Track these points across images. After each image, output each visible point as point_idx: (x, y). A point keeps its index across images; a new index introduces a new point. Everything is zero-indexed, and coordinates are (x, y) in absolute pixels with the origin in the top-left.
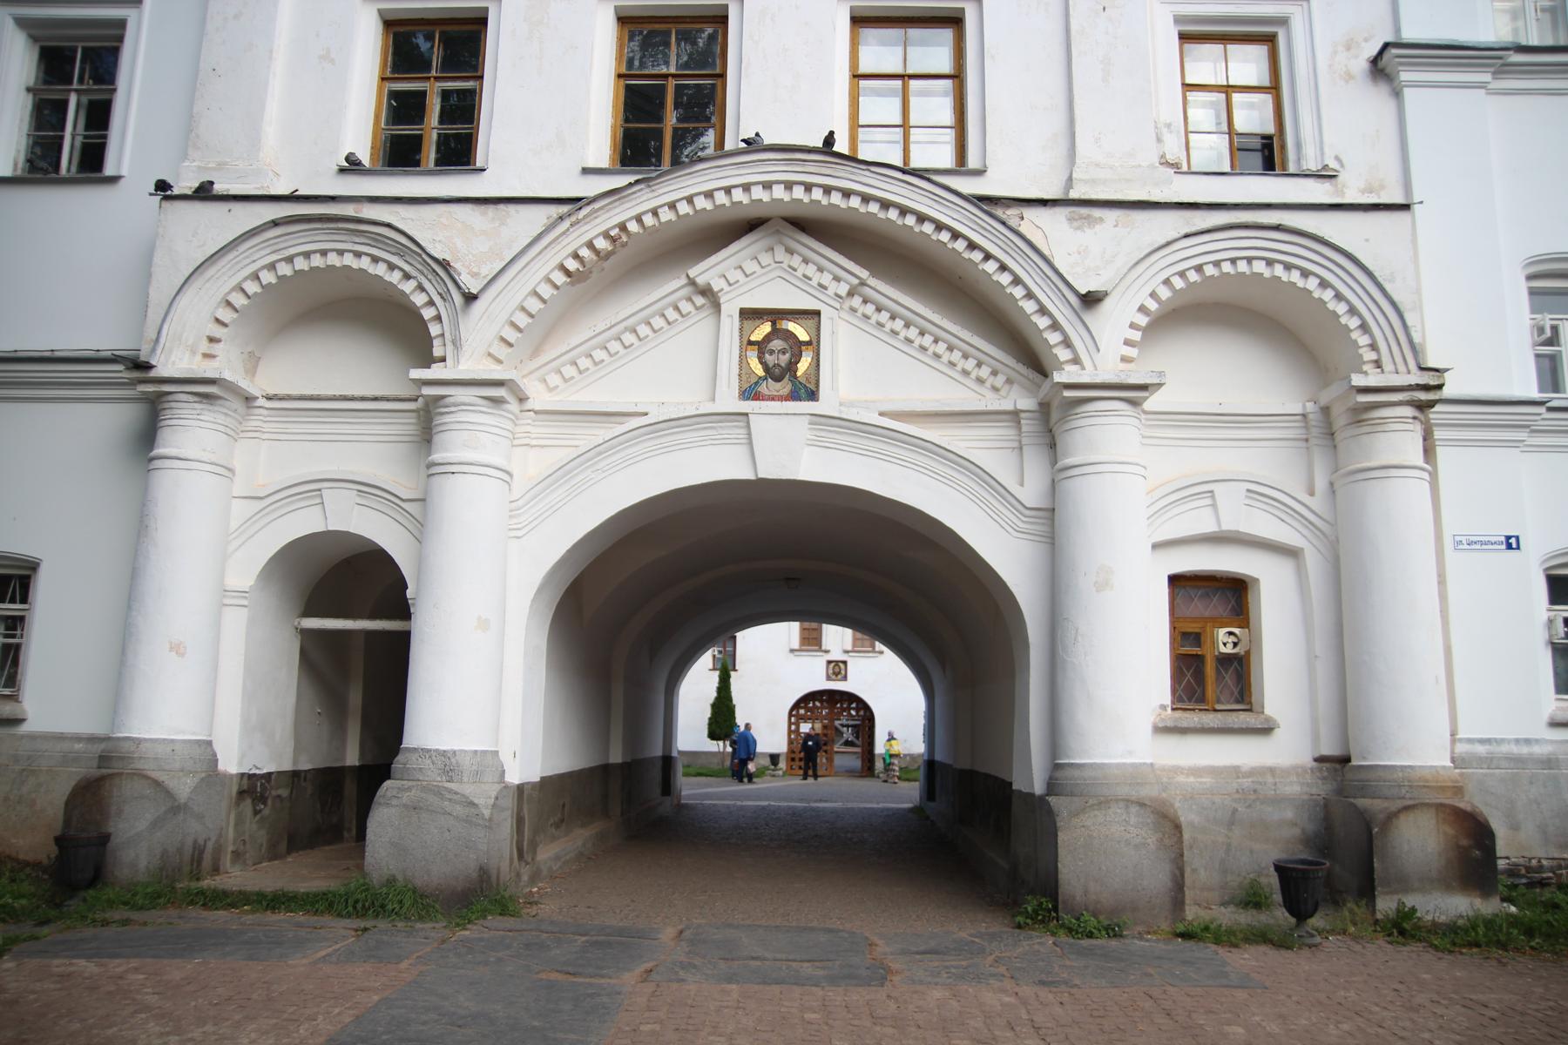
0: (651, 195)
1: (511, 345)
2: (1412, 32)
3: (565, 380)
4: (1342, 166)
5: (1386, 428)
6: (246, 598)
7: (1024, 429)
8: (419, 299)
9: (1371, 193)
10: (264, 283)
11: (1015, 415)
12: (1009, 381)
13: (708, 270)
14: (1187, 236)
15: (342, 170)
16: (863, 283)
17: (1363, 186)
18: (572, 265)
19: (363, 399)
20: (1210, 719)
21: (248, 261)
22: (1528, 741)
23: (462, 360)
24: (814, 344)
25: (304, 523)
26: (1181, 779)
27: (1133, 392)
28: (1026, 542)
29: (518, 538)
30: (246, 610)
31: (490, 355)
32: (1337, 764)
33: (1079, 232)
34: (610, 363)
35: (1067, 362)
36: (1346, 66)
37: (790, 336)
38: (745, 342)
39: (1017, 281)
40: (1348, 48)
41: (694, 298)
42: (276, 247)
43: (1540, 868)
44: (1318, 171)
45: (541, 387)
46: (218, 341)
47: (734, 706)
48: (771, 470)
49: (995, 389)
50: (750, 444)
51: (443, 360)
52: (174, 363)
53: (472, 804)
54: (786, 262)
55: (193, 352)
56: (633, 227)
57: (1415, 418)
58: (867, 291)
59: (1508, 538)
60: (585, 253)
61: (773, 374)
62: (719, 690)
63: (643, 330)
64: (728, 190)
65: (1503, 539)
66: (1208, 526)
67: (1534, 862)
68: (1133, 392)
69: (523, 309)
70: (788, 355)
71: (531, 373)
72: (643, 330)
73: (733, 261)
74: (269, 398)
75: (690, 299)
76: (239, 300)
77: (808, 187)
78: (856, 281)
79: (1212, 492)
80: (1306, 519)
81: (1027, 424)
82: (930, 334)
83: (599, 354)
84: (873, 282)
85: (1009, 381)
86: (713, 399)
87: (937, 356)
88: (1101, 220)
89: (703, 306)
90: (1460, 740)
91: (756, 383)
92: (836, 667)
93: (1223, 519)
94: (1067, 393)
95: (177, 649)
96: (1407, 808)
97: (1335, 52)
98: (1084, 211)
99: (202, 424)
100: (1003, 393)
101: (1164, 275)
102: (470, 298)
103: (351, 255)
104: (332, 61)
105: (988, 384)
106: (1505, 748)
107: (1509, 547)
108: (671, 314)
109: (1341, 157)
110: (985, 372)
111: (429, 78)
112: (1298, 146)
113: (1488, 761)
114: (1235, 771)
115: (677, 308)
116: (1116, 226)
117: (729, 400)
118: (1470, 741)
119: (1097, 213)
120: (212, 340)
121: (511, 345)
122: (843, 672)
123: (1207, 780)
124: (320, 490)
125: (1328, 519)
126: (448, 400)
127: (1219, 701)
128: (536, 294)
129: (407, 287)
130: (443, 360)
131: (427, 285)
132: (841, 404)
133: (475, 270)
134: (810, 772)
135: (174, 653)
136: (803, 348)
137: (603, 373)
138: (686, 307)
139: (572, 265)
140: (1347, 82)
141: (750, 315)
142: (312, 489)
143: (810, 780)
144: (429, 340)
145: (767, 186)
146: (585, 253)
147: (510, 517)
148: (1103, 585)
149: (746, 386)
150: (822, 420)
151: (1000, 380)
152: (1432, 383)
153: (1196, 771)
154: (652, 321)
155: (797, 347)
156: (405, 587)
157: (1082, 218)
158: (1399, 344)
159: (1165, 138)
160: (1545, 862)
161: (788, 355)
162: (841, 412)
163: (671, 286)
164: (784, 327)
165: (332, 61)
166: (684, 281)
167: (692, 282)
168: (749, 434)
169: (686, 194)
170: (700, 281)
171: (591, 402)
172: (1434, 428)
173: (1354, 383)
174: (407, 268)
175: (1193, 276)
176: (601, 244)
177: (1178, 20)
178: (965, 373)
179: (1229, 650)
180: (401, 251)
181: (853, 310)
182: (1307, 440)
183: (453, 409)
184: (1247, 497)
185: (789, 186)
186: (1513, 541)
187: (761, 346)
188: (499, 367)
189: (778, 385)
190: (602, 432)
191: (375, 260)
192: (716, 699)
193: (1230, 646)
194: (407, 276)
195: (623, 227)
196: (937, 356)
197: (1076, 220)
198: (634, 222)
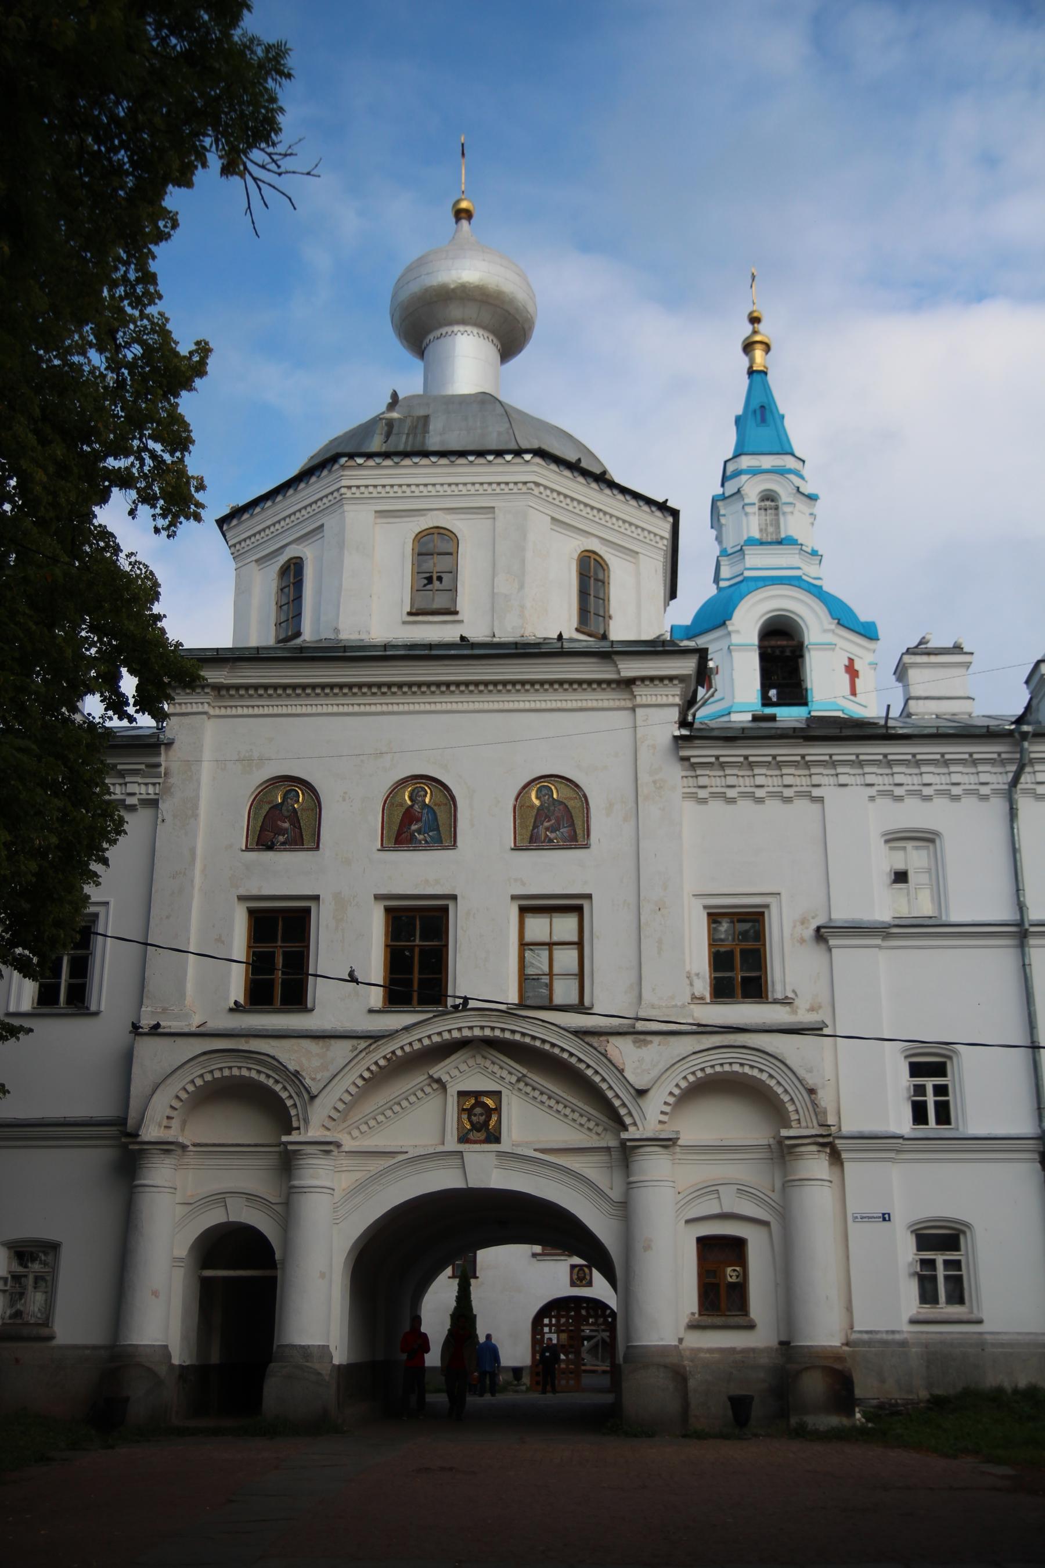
0: (408, 1035)
1: (334, 1120)
2: (841, 914)
3: (361, 1133)
4: (796, 995)
5: (803, 1157)
6: (183, 1262)
7: (613, 1157)
8: (284, 1095)
9: (813, 1011)
10: (197, 1085)
11: (608, 1149)
12: (605, 1129)
13: (439, 1070)
14: (694, 1053)
15: (231, 1010)
16: (524, 1076)
17: (808, 1007)
18: (367, 1075)
19: (249, 1145)
20: (718, 1320)
21: (188, 1074)
22: (893, 1332)
23: (309, 1131)
24: (498, 1110)
25: (215, 1217)
26: (702, 1355)
27: (668, 1143)
28: (613, 1220)
29: (337, 1224)
30: (182, 1269)
31: (323, 1126)
32: (785, 1345)
33: (639, 1050)
34: (386, 1123)
35: (631, 1124)
36: (801, 934)
37: (485, 1106)
38: (460, 1109)
39: (604, 1080)
40: (802, 923)
41: (432, 1085)
42: (204, 1066)
43: (897, 1405)
44: (783, 999)
45: (348, 1137)
46: (172, 1118)
47: (475, 1316)
48: (474, 1183)
49: (598, 1134)
50: (464, 1167)
51: (298, 1128)
52: (150, 1133)
53: (319, 1374)
54: (482, 1064)
55: (160, 1126)
56: (399, 1053)
57: (819, 1151)
58: (527, 1079)
59: (884, 1214)
60: (374, 1068)
61: (477, 1128)
62: (459, 1299)
63: (405, 1103)
64: (449, 1031)
65: (881, 1215)
66: (716, 1210)
67: (893, 1401)
68: (668, 1143)
69: (341, 1100)
70: (484, 1117)
71: (344, 1129)
72: (405, 1103)
73: (454, 1064)
74: (194, 1145)
75: (429, 1085)
76: (184, 1096)
77: (493, 1028)
78: (520, 1075)
79: (717, 1190)
80: (770, 1205)
81: (615, 1155)
82: (562, 1103)
83: (380, 1118)
84: (529, 1075)
85: (605, 1129)
86: (443, 1144)
87: (566, 1116)
88: (651, 1042)
89: (437, 1089)
90: (855, 1332)
91: (467, 1133)
92: (581, 1272)
93: (723, 1208)
94: (628, 1144)
95: (155, 1294)
96: (807, 1369)
97: (795, 927)
98: (642, 1037)
99: (165, 1166)
100: (602, 1136)
101: (683, 1074)
102: (313, 1098)
103: (245, 1069)
104: (223, 942)
105: (594, 1131)
106: (879, 1336)
107: (884, 1219)
108: (420, 1094)
109: (796, 991)
110: (591, 1125)
111: (277, 947)
112: (773, 983)
113: (868, 1343)
114: (732, 1351)
115: (422, 1090)
116: (659, 1045)
117: (452, 1143)
118: (860, 1332)
119: (649, 1038)
120: (168, 1118)
121: (334, 1120)
122: (588, 1277)
123: (716, 1355)
124: (224, 1198)
125: (782, 1204)
126: (302, 1152)
127: (729, 1310)
128: (347, 1091)
129: (278, 1088)
130: (298, 1128)
131: (289, 1088)
132: (513, 1145)
133: (313, 1076)
134: (549, 1388)
135: (153, 1296)
136: (493, 1112)
137: (382, 1128)
138: (428, 1090)
139: (367, 1075)
140: (801, 944)
141: (461, 1094)
142: (220, 1198)
143: (549, 1395)
144: (289, 1118)
145: (471, 1028)
146: (374, 1068)
147: (334, 1212)
148: (647, 1248)
149: (461, 1135)
150: (504, 1154)
151: (600, 1129)
152: (824, 1133)
153: (710, 1351)
154: (409, 1098)
155: (488, 1111)
156: (273, 1253)
157: (641, 1041)
158: (808, 1111)
159: (694, 984)
160: (899, 1401)
161: (484, 1117)
162: (513, 1149)
163: (418, 1079)
164: (482, 1100)
165: (223, 942)
166: (426, 1076)
167: (431, 1077)
168: (463, 1162)
169: (427, 1034)
170: (435, 1076)
171: (376, 1145)
172: (842, 1152)
173: (782, 1135)
174: (277, 1077)
175: (700, 1074)
176: (382, 1062)
177: (705, 907)
178: (581, 1125)
179: (734, 1280)
180: (274, 1069)
181: (520, 1090)
182: (772, 1159)
183: (305, 1157)
184: (737, 1193)
185: (482, 1028)
186: (887, 1216)
187: (470, 1112)
188: (328, 1133)
189: (479, 1134)
190: (382, 1162)
191: (259, 1072)
192: (456, 1308)
193: (734, 1277)
194: (277, 1082)
195: (393, 1052)
196: (566, 1116)
197: (638, 1042)
198: (399, 1050)
